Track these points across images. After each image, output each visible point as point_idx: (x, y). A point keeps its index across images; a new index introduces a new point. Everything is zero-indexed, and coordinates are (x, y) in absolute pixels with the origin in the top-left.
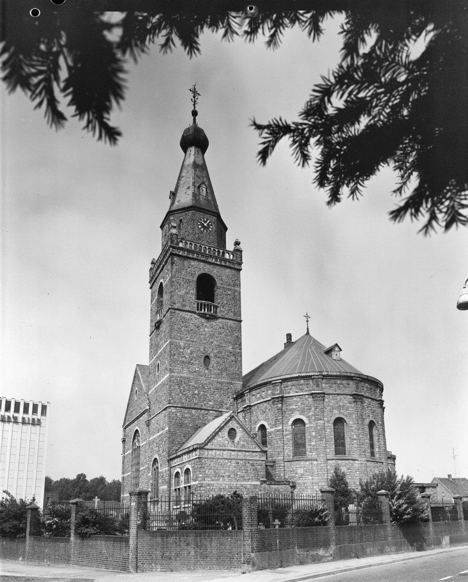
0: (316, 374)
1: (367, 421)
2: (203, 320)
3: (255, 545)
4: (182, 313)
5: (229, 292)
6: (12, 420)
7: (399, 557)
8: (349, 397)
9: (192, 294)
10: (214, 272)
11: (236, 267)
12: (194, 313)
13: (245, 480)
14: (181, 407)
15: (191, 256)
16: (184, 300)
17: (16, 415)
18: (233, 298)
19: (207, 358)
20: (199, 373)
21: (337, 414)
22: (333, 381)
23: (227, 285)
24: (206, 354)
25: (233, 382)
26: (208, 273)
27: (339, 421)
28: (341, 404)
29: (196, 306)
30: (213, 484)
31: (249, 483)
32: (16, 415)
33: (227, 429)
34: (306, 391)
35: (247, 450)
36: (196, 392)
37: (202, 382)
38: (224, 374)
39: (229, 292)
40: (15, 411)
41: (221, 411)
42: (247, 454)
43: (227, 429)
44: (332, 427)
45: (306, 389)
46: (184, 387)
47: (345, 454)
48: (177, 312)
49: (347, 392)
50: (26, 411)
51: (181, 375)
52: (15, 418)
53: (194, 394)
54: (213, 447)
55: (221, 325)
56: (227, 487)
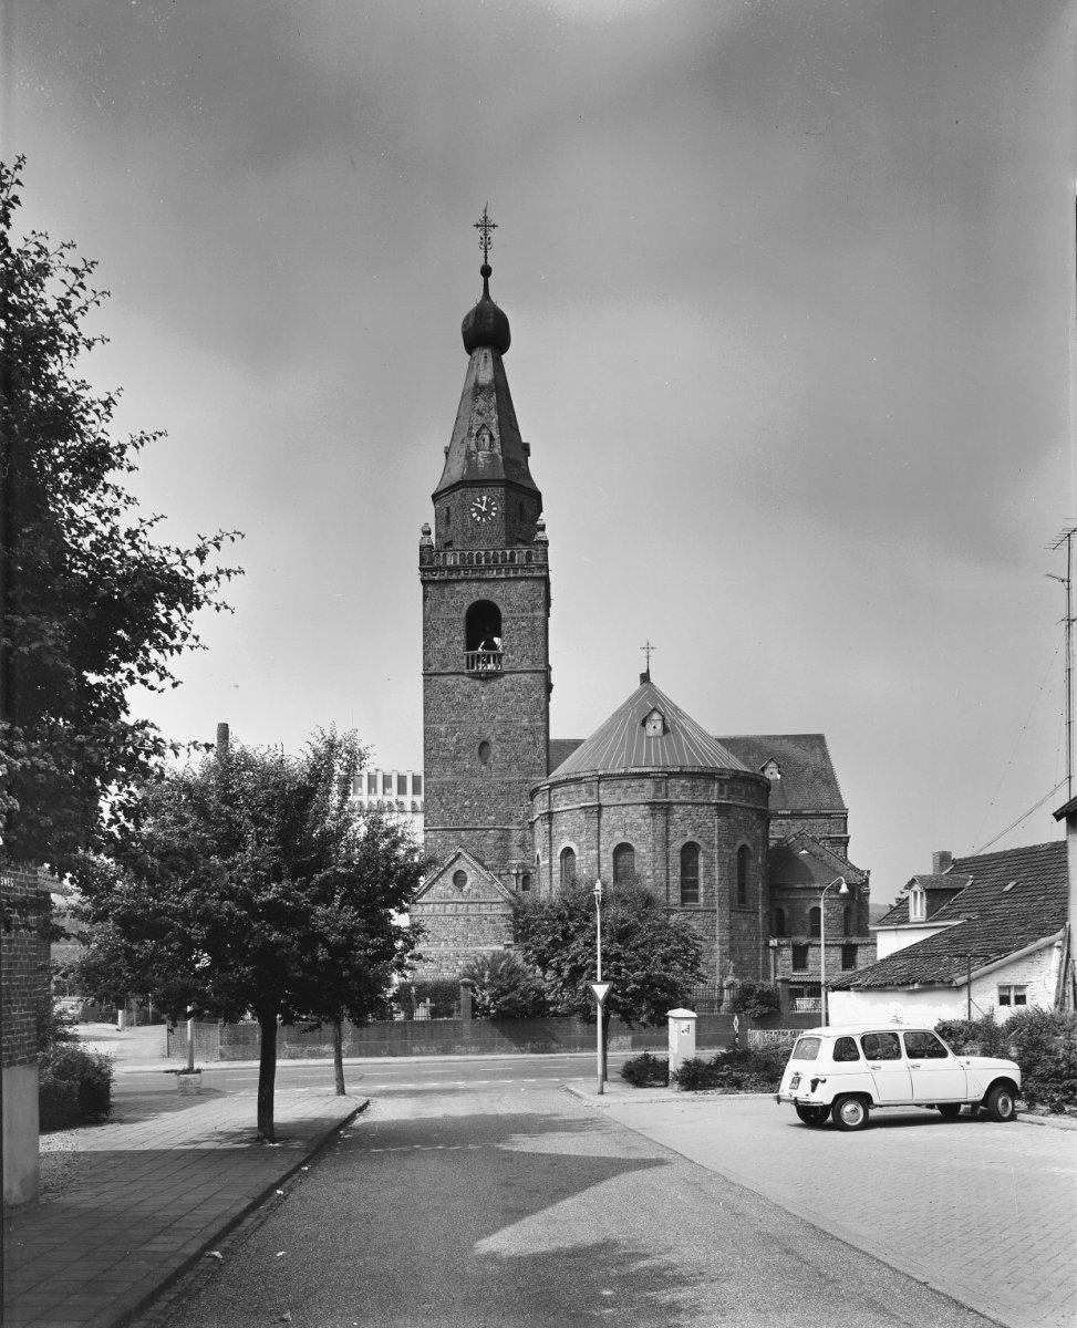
0: (588, 774)
1: (678, 845)
2: (478, 683)
3: (224, 1038)
4: (443, 680)
5: (524, 624)
6: (396, 808)
8: (642, 807)
10: (494, 593)
12: (463, 674)
14: (444, 830)
15: (454, 577)
16: (444, 656)
17: (401, 798)
18: (531, 633)
19: (484, 744)
20: (471, 773)
21: (619, 838)
22: (615, 784)
25: (530, 779)
26: (486, 598)
27: (623, 849)
28: (628, 821)
29: (464, 661)
31: (486, 948)
32: (401, 798)
33: (451, 873)
34: (577, 803)
35: (483, 900)
36: (466, 803)
38: (515, 767)
39: (524, 624)
40: (414, 793)
41: (507, 829)
42: (483, 906)
43: (452, 873)
44: (612, 860)
45: (577, 800)
48: (434, 678)
49: (639, 800)
50: (402, 790)
51: (442, 779)
52: (401, 804)
54: (430, 900)
55: (508, 685)
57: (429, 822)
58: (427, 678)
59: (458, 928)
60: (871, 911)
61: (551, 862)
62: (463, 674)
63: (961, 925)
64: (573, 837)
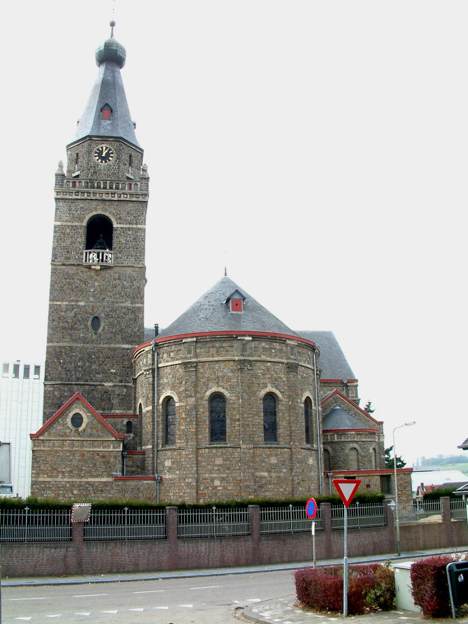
7: (78, 580)
9: (79, 242)
11: (141, 199)
13: (93, 476)
16: (68, 252)
19: (96, 320)
20: (85, 341)
23: (126, 224)
24: (97, 315)
30: (49, 482)
37: (88, 350)
46: (64, 359)
47: (225, 440)
53: (76, 367)
56: (68, 485)
57: (49, 377)
58: (55, 267)
59: (75, 462)
60: (357, 491)
61: (153, 408)
62: (81, 265)
63: (191, 587)
64: (173, 388)
